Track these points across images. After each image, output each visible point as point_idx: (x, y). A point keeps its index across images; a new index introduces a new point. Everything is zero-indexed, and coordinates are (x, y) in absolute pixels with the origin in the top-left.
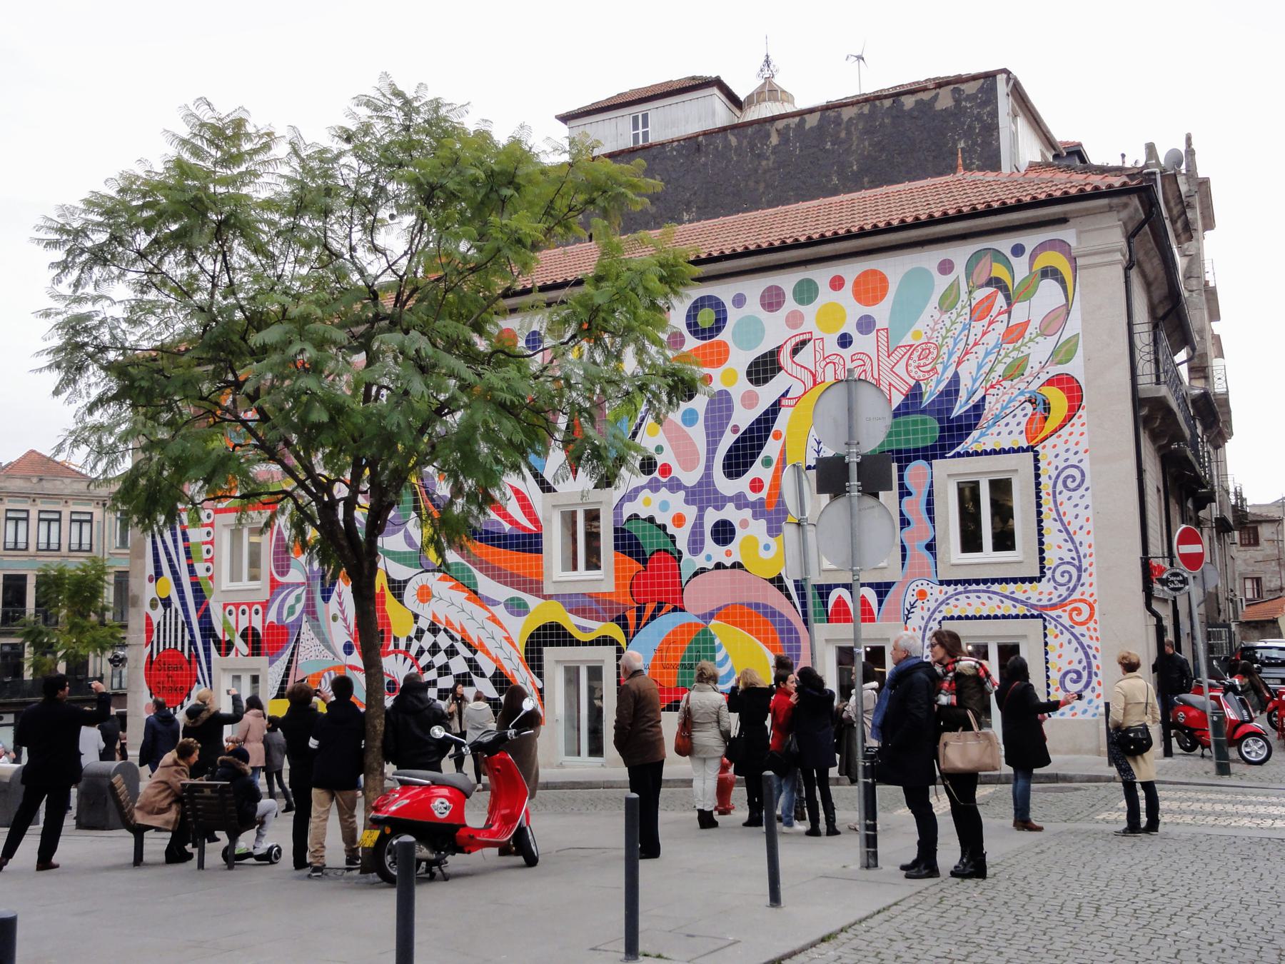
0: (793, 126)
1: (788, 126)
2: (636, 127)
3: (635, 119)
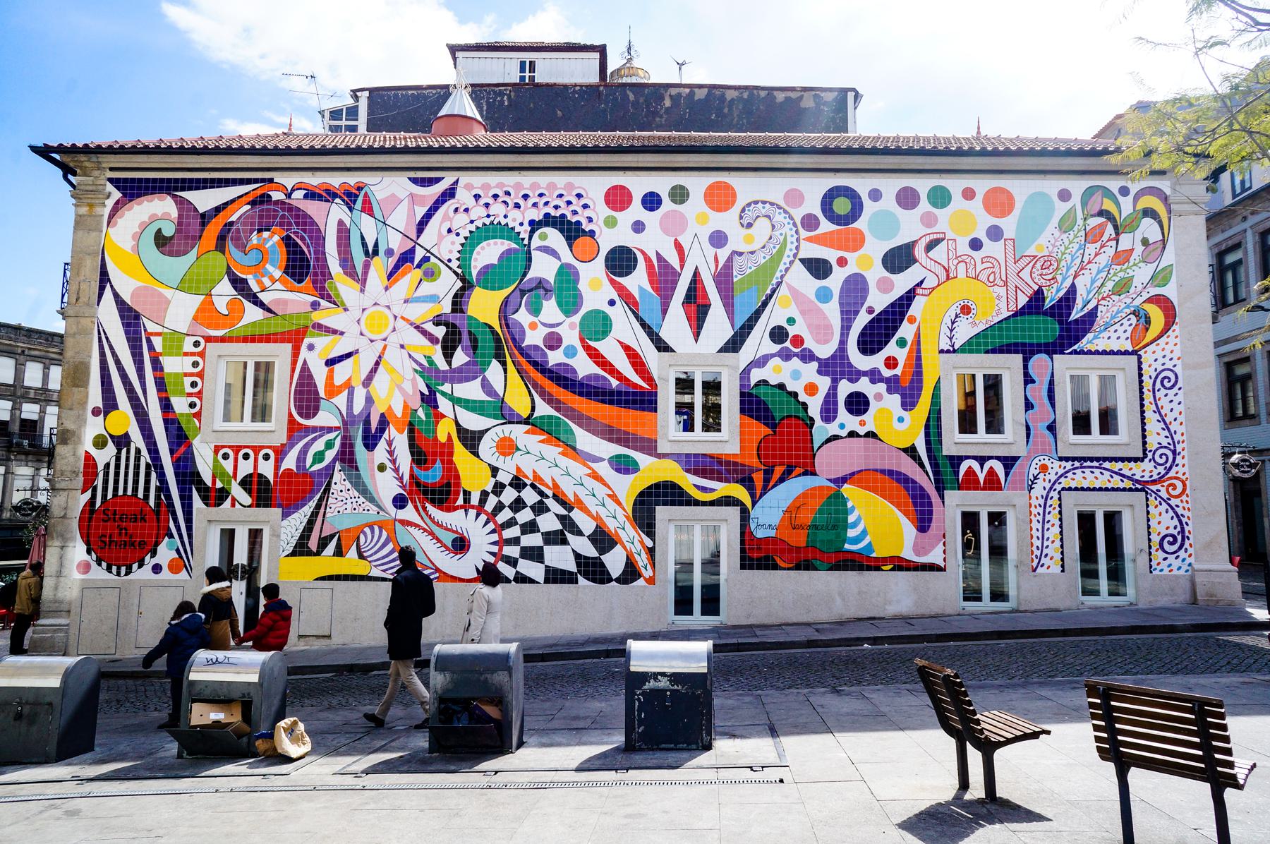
0: (729, 98)
1: (679, 95)
2: (522, 70)
3: (523, 64)
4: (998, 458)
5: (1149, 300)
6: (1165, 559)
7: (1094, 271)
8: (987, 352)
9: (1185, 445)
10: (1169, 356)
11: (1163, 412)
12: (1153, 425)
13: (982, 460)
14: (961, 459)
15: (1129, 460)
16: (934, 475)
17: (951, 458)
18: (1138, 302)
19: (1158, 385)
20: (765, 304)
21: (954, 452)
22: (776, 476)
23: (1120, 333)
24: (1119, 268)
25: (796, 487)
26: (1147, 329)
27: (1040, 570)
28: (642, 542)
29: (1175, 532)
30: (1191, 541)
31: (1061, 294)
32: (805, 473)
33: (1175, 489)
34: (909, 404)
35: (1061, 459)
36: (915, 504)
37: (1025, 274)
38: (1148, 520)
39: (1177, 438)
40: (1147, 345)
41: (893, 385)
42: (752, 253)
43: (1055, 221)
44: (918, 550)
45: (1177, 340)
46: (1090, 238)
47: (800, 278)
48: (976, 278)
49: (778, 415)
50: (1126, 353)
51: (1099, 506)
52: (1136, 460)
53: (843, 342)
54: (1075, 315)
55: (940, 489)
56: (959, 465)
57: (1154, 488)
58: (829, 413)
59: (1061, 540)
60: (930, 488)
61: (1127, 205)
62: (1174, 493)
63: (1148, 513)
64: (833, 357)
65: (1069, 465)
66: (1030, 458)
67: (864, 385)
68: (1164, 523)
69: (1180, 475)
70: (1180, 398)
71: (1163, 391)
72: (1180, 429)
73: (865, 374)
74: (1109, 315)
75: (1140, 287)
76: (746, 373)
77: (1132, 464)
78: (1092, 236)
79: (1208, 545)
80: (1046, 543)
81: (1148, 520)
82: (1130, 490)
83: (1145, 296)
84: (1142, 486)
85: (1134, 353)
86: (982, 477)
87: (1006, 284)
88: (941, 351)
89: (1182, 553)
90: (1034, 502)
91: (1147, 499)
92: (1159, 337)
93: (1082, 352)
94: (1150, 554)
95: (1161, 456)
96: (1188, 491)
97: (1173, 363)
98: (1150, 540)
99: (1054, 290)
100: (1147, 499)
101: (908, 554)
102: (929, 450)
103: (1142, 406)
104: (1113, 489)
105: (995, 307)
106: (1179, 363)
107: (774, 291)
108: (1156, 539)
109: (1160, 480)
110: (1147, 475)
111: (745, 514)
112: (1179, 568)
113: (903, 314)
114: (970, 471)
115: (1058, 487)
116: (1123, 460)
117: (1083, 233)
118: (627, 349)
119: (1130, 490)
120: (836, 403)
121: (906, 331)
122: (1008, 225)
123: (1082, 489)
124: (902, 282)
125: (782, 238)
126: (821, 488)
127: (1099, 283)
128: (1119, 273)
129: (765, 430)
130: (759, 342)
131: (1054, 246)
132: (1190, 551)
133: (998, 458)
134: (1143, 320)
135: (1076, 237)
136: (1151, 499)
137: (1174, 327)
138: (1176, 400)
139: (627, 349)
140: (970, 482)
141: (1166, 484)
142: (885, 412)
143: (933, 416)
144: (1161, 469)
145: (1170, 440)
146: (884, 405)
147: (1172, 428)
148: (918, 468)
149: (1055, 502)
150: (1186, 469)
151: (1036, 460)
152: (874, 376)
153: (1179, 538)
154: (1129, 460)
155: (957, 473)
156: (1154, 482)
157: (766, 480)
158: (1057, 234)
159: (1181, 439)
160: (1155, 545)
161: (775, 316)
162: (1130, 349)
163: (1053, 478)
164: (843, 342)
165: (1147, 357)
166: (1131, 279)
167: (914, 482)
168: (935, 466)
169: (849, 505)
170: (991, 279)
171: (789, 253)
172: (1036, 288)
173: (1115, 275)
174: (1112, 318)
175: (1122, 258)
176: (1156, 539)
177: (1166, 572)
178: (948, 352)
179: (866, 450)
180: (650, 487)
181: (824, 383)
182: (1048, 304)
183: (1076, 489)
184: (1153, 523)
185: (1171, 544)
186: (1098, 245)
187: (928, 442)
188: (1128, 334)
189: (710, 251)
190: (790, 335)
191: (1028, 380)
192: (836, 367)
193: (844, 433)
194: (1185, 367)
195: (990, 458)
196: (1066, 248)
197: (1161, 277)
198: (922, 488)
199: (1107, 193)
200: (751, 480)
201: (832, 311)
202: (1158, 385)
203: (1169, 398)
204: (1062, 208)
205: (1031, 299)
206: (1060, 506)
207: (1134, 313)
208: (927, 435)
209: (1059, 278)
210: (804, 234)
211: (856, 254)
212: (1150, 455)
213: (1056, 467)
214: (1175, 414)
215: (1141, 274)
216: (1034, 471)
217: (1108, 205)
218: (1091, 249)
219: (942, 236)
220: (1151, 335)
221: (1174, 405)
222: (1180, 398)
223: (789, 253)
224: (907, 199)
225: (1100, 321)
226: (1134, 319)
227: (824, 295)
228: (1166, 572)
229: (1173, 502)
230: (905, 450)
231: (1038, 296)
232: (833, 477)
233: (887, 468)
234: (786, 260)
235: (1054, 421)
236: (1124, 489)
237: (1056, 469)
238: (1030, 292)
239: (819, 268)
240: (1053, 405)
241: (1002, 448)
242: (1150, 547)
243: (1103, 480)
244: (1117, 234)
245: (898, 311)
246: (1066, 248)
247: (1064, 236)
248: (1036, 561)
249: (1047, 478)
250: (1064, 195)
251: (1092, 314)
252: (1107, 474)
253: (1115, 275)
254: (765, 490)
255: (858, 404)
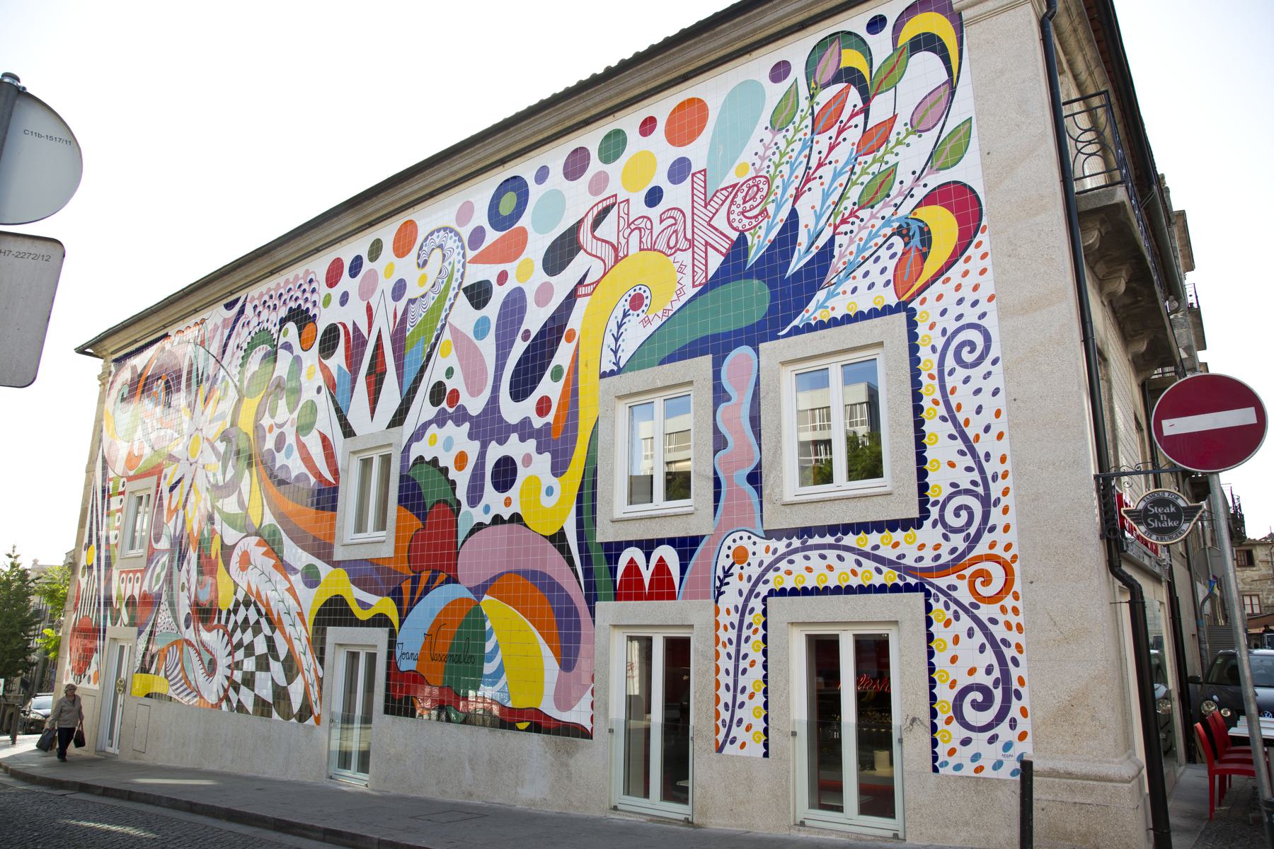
4: (671, 542)
5: (928, 200)
6: (966, 742)
7: (827, 180)
8: (662, 363)
9: (1008, 482)
10: (970, 297)
11: (961, 417)
12: (941, 448)
13: (648, 546)
14: (621, 546)
15: (893, 525)
16: (585, 577)
17: (607, 546)
18: (905, 210)
19: (950, 362)
20: (429, 357)
21: (610, 538)
22: (422, 585)
23: (875, 276)
24: (869, 158)
25: (441, 596)
26: (924, 257)
27: (728, 749)
28: (315, 671)
29: (988, 681)
30: (1025, 702)
31: (773, 235)
32: (448, 581)
33: (986, 583)
34: (559, 468)
35: (769, 535)
36: (559, 624)
37: (720, 222)
38: (931, 654)
39: (990, 468)
40: (926, 286)
41: (545, 440)
42: (423, 296)
43: (765, 119)
44: (564, 699)
45: (987, 263)
46: (820, 127)
47: (463, 315)
48: (653, 249)
49: (429, 501)
50: (887, 310)
51: (848, 621)
52: (906, 524)
53: (496, 389)
54: (797, 263)
55: (591, 599)
56: (617, 557)
57: (942, 582)
58: (475, 495)
59: (765, 691)
60: (578, 597)
61: (881, 45)
62: (986, 591)
63: (930, 637)
64: (485, 411)
65: (781, 546)
66: (720, 537)
67: (515, 448)
68: (964, 661)
69: (998, 551)
70: (997, 380)
71: (961, 373)
72: (998, 449)
73: (514, 428)
74: (853, 248)
75: (909, 181)
76: (407, 449)
77: (899, 535)
78: (824, 120)
79: (1066, 713)
80: (740, 698)
81: (931, 654)
82: (895, 589)
83: (920, 193)
84: (917, 582)
85: (902, 307)
86: (647, 576)
87: (692, 243)
88: (603, 375)
89: (1003, 730)
90: (724, 619)
91: (929, 608)
92: (949, 264)
93: (809, 328)
94: (934, 728)
95: (957, 515)
96: (1017, 587)
97: (979, 310)
98: (933, 698)
99: (762, 233)
100: (929, 608)
101: (549, 707)
102: (580, 536)
103: (918, 409)
104: (862, 590)
105: (674, 282)
106: (991, 308)
107: (437, 338)
108: (945, 695)
109: (954, 566)
110: (928, 554)
111: (392, 634)
112: (998, 765)
113: (561, 329)
114: (632, 568)
115: (763, 590)
116: (879, 526)
117: (809, 121)
118: (324, 439)
119: (895, 589)
120: (483, 475)
121: (563, 355)
122: (697, 152)
123: (805, 592)
124: (564, 282)
125: (450, 268)
126: (461, 600)
127: (835, 197)
128: (871, 165)
129: (417, 523)
130: (422, 409)
131: (763, 159)
132: (1024, 724)
133: (671, 542)
134: (916, 241)
135: (797, 131)
136: (938, 606)
137: (979, 237)
138: (988, 386)
139: (324, 439)
140: (631, 588)
141: (968, 572)
142: (534, 481)
143: (589, 479)
144: (958, 541)
145: (975, 476)
146: (536, 470)
147: (981, 449)
148: (566, 567)
149: (755, 618)
150: (1012, 536)
151: (729, 541)
152: (524, 429)
153: (998, 694)
154: (893, 525)
155: (613, 571)
156: (943, 570)
157: (413, 591)
158: (768, 136)
159: (1000, 469)
160: (944, 711)
161: (434, 374)
162: (893, 301)
163: (755, 571)
164: (496, 389)
165: (926, 310)
166: (893, 170)
167: (561, 589)
168: (586, 560)
169: (488, 625)
170: (672, 244)
171: (455, 284)
172: (734, 235)
173: (864, 172)
174: (860, 251)
175: (875, 139)
176: (945, 695)
177: (968, 770)
178: (612, 373)
179: (510, 542)
180: (325, 604)
181: (473, 449)
182: (753, 257)
183: (794, 592)
184: (940, 660)
185: (977, 706)
186: (833, 132)
187: (580, 524)
188: (889, 275)
189: (391, 304)
190: (448, 391)
191: (720, 395)
192: (488, 426)
193: (487, 519)
194: (1003, 314)
195: (660, 542)
196: (782, 156)
197: (949, 150)
198: (569, 599)
199: (848, 38)
200: (400, 591)
201: (488, 347)
202: (950, 362)
203: (972, 385)
204: (775, 92)
205: (727, 256)
206: (765, 626)
207: (899, 232)
208: (579, 511)
209: (771, 208)
210: (471, 254)
211: (516, 263)
212: (934, 512)
213: (761, 552)
214: (987, 416)
215: (910, 155)
216: (724, 562)
217: (851, 58)
218: (823, 141)
219: (612, 200)
220: (931, 267)
221: (985, 398)
222: (997, 380)
223: (455, 284)
224: (576, 165)
225: (837, 263)
226: (898, 243)
227: (481, 329)
228: (968, 770)
229: (984, 612)
230: (552, 539)
231: (739, 247)
232: (473, 584)
233: (530, 568)
234: (451, 294)
235: (759, 466)
236: (882, 589)
237: (762, 554)
238: (725, 246)
239: (478, 295)
240: (758, 435)
241: (676, 521)
242: (934, 714)
243: (842, 571)
244: (867, 100)
245: (554, 331)
246: (782, 156)
247: (779, 138)
248: (723, 731)
249: (745, 573)
250: (780, 71)
251: (826, 253)
252: (850, 558)
253: (864, 172)
254: (412, 604)
255: (505, 474)
